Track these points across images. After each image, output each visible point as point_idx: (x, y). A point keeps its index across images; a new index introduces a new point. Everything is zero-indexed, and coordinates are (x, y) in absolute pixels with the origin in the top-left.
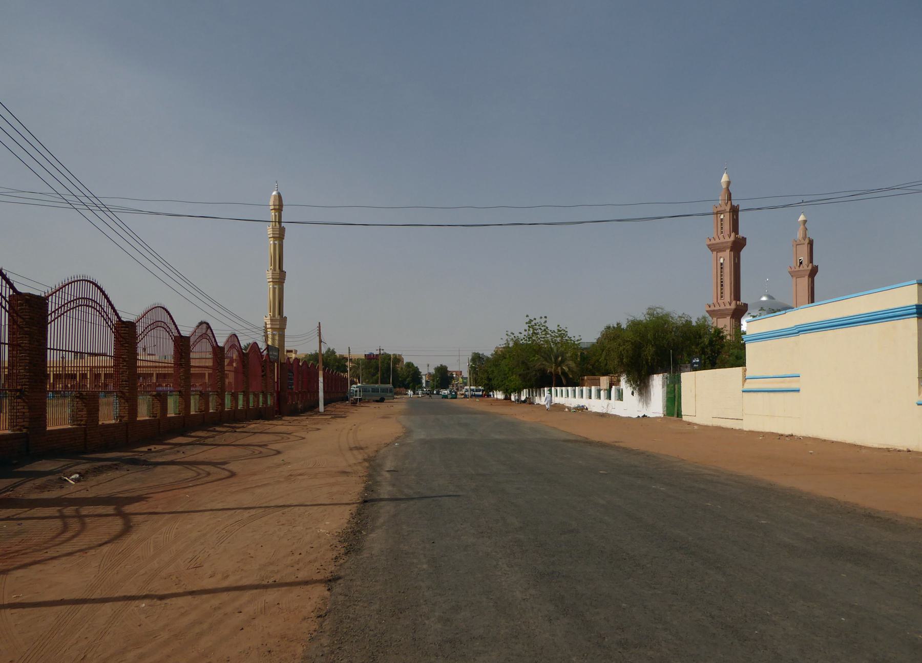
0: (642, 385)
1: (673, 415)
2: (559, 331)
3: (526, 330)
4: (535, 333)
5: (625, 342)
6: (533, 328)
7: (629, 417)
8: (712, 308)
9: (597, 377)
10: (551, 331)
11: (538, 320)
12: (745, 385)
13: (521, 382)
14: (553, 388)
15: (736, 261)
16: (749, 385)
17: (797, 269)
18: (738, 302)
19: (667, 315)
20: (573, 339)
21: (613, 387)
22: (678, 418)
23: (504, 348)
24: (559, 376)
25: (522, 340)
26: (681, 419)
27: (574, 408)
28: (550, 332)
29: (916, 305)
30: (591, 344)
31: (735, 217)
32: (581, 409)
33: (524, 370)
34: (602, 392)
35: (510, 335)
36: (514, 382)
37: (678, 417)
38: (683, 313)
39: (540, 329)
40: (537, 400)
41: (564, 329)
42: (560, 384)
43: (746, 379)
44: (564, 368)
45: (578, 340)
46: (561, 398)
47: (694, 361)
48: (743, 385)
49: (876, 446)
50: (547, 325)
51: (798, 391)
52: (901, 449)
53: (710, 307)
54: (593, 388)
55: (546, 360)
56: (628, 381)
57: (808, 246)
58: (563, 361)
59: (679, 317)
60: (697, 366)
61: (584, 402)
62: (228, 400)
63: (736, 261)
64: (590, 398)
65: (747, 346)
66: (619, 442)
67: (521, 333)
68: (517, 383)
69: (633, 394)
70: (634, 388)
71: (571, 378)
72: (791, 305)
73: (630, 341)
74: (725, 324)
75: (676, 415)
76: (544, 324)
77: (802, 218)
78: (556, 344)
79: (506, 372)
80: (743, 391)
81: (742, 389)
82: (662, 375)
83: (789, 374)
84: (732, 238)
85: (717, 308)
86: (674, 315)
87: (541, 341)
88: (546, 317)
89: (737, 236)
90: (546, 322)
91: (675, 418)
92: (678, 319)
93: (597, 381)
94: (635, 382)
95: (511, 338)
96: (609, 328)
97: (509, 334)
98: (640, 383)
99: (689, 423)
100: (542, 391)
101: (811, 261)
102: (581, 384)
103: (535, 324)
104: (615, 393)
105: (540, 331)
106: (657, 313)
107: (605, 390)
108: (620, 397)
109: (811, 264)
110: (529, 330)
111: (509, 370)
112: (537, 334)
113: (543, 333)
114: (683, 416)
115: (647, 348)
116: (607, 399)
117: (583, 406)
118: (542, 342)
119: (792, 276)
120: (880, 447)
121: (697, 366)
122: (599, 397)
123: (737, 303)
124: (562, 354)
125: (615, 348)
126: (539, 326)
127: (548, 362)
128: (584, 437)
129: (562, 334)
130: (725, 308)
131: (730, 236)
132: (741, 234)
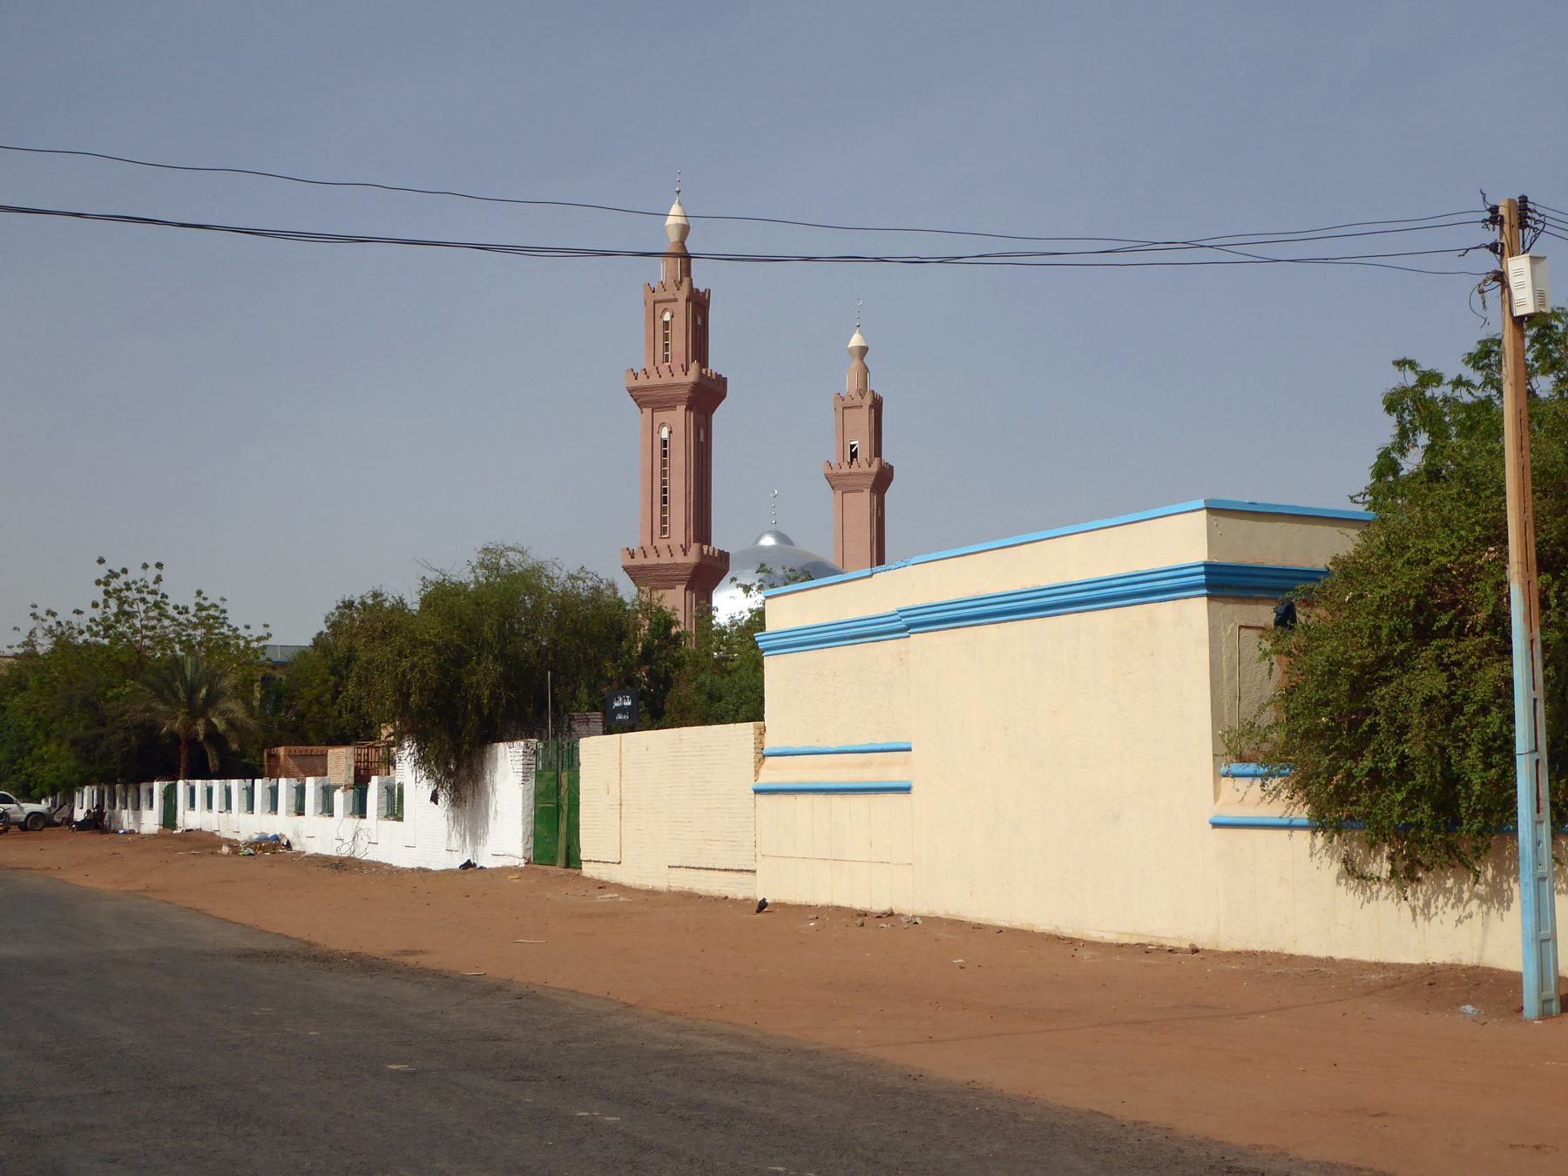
0: (464, 772)
1: (553, 863)
2: (200, 608)
3: (95, 605)
4: (125, 613)
5: (417, 644)
6: (119, 599)
7: (420, 869)
8: (639, 560)
9: (316, 749)
10: (176, 607)
11: (135, 574)
12: (763, 771)
13: (73, 763)
14: (181, 784)
15: (702, 439)
16: (776, 772)
17: (846, 469)
18: (705, 548)
19: (537, 571)
20: (242, 632)
21: (375, 780)
22: (569, 870)
23: (16, 656)
24: (200, 744)
25: (81, 632)
26: (577, 872)
27: (249, 844)
28: (173, 613)
29: (1206, 565)
30: (298, 650)
31: (699, 322)
32: (272, 846)
33: (86, 727)
34: (339, 797)
35: (45, 617)
36: (53, 765)
37: (567, 866)
38: (582, 568)
39: (143, 600)
40: (126, 818)
41: (218, 603)
42: (200, 770)
43: (764, 756)
44: (215, 720)
45: (259, 639)
46: (206, 812)
47: (616, 704)
48: (757, 772)
49: (1110, 937)
50: (163, 588)
51: (906, 790)
52: (1174, 944)
53: (633, 557)
54: (311, 783)
55: (159, 695)
56: (422, 761)
57: (870, 412)
58: (211, 700)
59: (571, 577)
60: (626, 717)
61: (280, 824)
62: (1541, 713)
63: (702, 439)
64: (300, 811)
65: (766, 661)
66: (414, 953)
67: (78, 612)
68: (64, 765)
69: (434, 798)
70: (438, 782)
71: (235, 753)
72: (830, 557)
73: (431, 643)
74: (675, 600)
75: (561, 861)
76: (156, 587)
77: (856, 340)
78: (188, 646)
79: (28, 732)
80: (757, 792)
81: (752, 785)
82: (522, 743)
83: (881, 740)
84: (692, 376)
85: (652, 560)
86: (557, 571)
87: (144, 637)
88: (159, 565)
89: (704, 370)
90: (158, 580)
91: (558, 870)
92: (568, 585)
93: (317, 761)
94: (442, 762)
95: (46, 625)
96: (349, 605)
97: (41, 613)
98: (458, 767)
99: (602, 886)
100: (144, 795)
101: (877, 450)
102: (272, 771)
103: (127, 584)
104: (379, 797)
105: (142, 607)
106: (509, 565)
107: (347, 787)
108: (394, 808)
109: (876, 461)
110: (106, 606)
111: (37, 726)
112: (131, 615)
113: (151, 614)
114: (584, 865)
115: (478, 663)
116: (352, 814)
117: (276, 838)
118: (147, 642)
119: (833, 488)
120: (1122, 941)
121: (626, 717)
122: (328, 809)
123: (702, 549)
124: (212, 678)
125: (388, 663)
126: (139, 591)
127: (167, 702)
128: (301, 941)
129: (210, 617)
130: (672, 561)
131: (687, 369)
132: (716, 365)
